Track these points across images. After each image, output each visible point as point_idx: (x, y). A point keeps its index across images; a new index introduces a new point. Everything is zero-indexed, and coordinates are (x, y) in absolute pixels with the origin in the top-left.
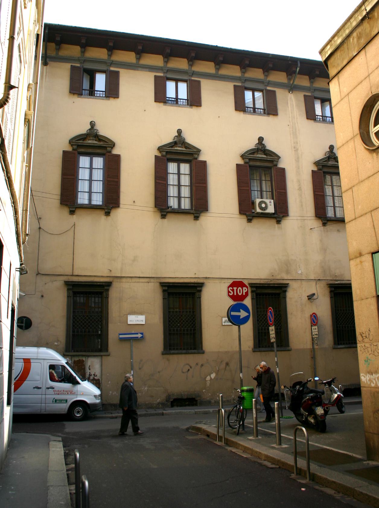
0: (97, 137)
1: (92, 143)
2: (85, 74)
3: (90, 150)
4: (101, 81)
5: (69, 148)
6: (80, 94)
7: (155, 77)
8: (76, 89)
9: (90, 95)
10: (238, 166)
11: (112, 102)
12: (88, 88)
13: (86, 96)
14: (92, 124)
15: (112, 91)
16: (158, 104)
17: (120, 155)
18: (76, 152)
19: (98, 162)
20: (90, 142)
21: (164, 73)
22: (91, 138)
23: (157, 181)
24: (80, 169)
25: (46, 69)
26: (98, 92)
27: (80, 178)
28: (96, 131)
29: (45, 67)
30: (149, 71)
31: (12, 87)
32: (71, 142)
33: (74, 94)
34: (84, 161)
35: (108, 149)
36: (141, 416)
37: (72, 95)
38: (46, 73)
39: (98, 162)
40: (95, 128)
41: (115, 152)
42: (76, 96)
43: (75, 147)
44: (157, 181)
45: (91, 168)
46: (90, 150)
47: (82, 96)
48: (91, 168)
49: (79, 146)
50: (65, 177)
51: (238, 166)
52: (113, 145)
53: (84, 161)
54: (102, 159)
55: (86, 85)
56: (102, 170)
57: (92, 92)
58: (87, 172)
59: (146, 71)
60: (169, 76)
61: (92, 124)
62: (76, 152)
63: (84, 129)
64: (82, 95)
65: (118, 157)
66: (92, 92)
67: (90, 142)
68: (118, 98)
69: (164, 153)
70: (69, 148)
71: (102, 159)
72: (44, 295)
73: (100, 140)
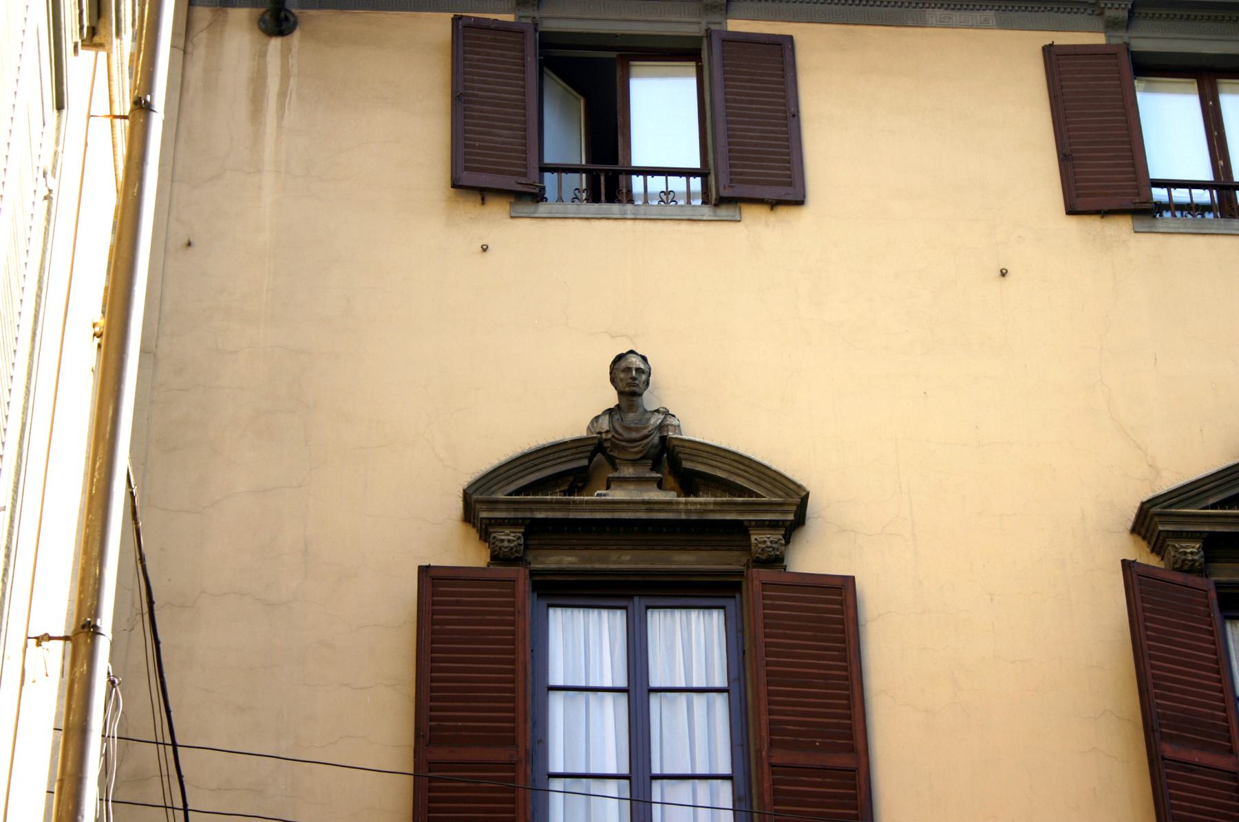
0: (672, 458)
1: (637, 512)
2: (555, 89)
3: (623, 560)
4: (664, 116)
5: (461, 551)
6: (527, 196)
7: (1050, 52)
8: (490, 171)
9: (594, 198)
10: (431, 579)
11: (757, 231)
12: (578, 156)
13: (572, 208)
14: (629, 376)
15: (754, 164)
16: (1093, 224)
17: (851, 580)
18: (520, 575)
19: (690, 644)
20: (617, 494)
21: (1111, 26)
22: (628, 471)
23: (1168, 750)
24: (557, 703)
25: (285, 54)
26: (657, 184)
27: (557, 766)
28: (656, 420)
29: (275, 43)
30: (1003, 25)
31: (45, 198)
32: (480, 504)
33: (484, 193)
34: (581, 643)
35: (756, 537)
36: (262, 55)
37: (470, 208)
38: (285, 76)
39: (690, 644)
40: (650, 400)
41: (812, 557)
42: (498, 210)
43: (509, 537)
44: (1168, 750)
45: (638, 691)
46: (623, 560)
47: (543, 208)
48: (638, 691)
49: (541, 532)
50: (441, 754)
51: (431, 579)
52: (791, 509)
53: (581, 643)
54: (716, 619)
55: (563, 140)
56: (720, 702)
57: (607, 176)
58: (610, 717)
59: (984, 25)
60: (1151, 39)
61: (629, 376)
62: (520, 575)
63: (571, 406)
64: (538, 196)
65: (840, 591)
66: (607, 176)
67: (617, 494)
68: (799, 202)
69: (1192, 548)
70: (461, 551)
71: (716, 619)
72: (487, 254)
73: (690, 483)
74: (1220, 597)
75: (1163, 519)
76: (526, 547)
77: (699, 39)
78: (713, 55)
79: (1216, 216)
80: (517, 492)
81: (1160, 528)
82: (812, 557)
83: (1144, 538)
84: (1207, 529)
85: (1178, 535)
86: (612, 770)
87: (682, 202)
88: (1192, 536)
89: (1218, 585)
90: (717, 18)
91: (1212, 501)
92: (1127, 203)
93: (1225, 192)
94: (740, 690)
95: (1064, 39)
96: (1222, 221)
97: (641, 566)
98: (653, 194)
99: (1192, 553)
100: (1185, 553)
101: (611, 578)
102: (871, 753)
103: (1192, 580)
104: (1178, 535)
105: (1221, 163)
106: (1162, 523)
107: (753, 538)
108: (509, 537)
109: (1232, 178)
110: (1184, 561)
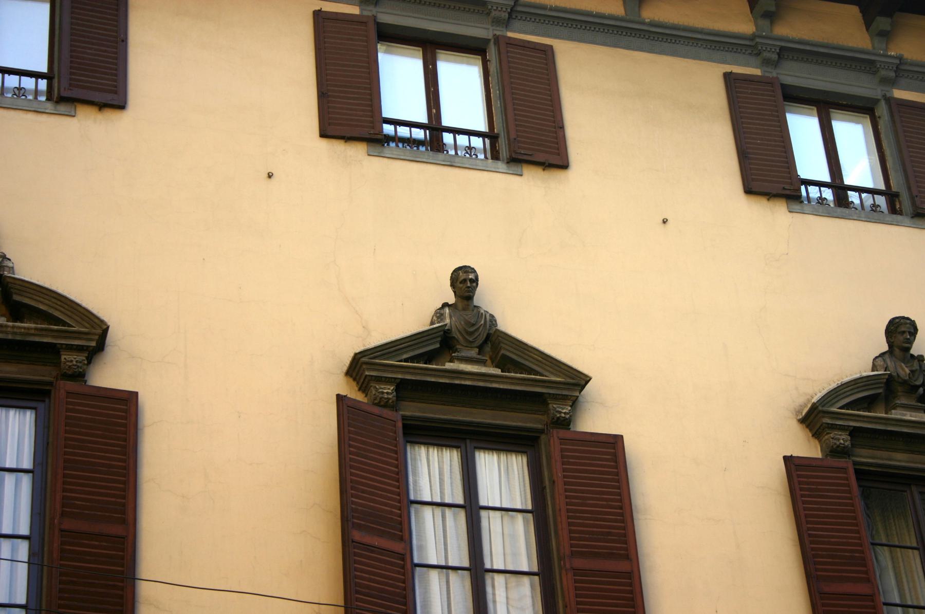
75: (368, 367)
77: (487, 41)
81: (367, 373)
84: (400, 376)
85: (379, 380)
88: (388, 381)
91: (405, 356)
103: (387, 413)
104: (379, 380)
106: (369, 369)
110: (558, 418)
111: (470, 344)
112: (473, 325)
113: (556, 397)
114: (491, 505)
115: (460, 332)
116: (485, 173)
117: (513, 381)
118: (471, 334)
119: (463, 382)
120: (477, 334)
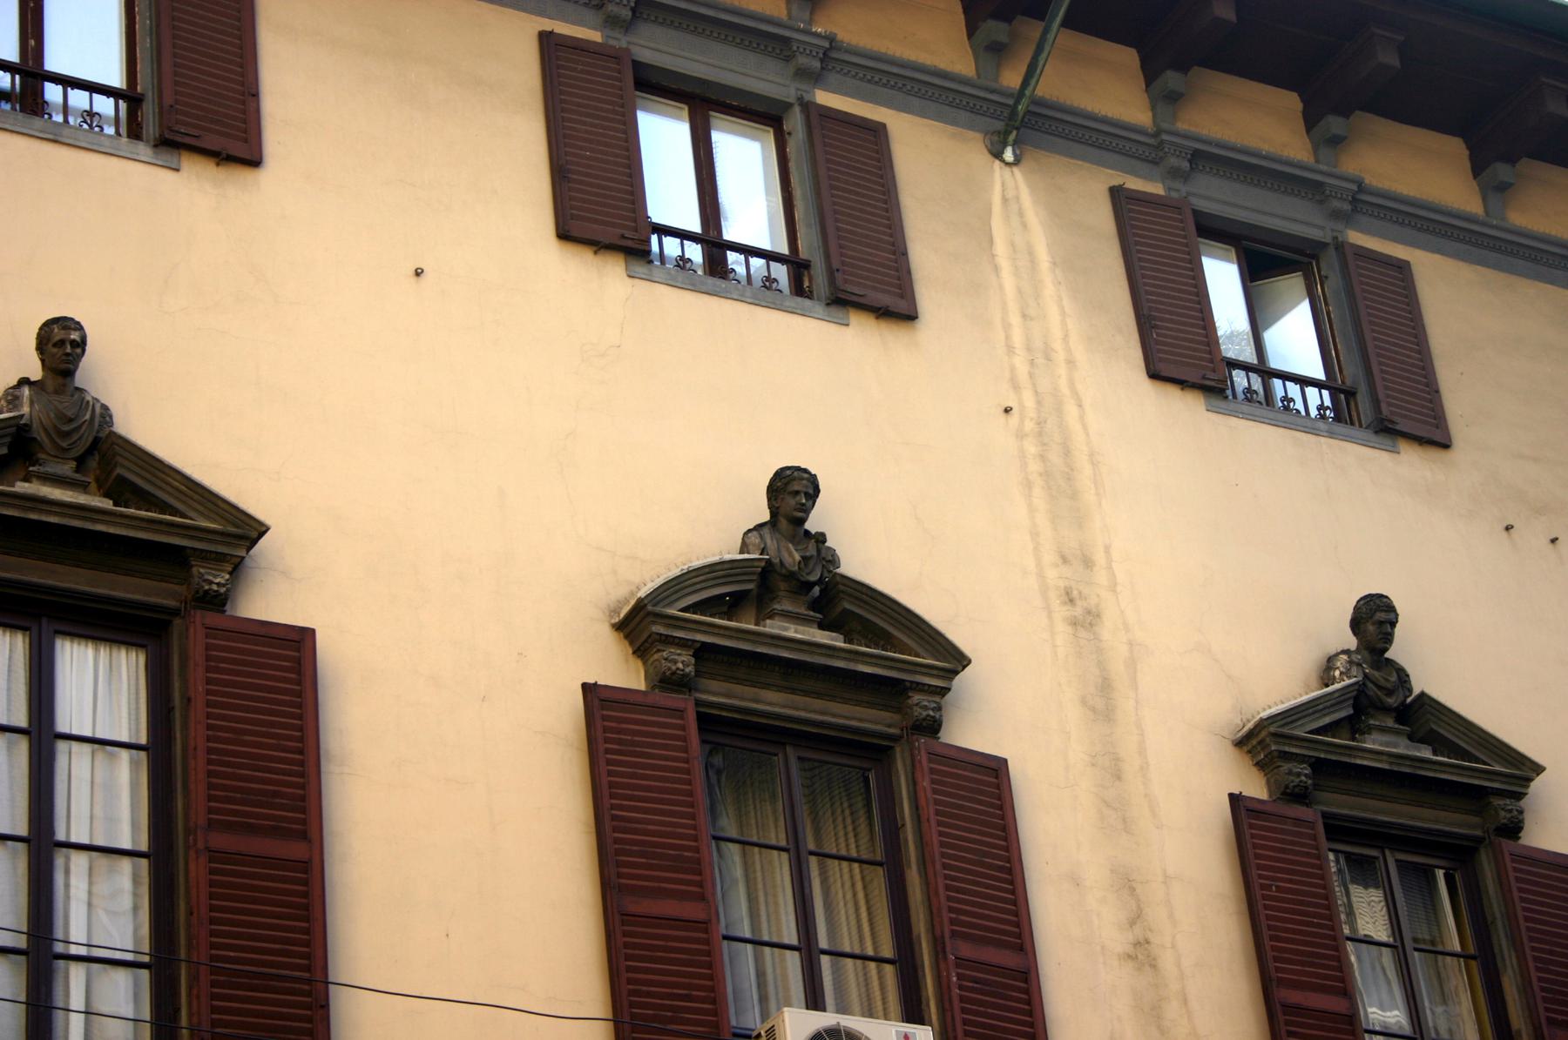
0: (1423, 717)
7: (545, 38)
15: (850, 264)
21: (612, 22)
35: (199, 570)
61: (61, 344)
68: (253, 161)
70: (621, 671)
73: (121, 491)
74: (701, 718)
76: (698, 673)
78: (1329, 265)
79: (14, 109)
80: (1317, 731)
82: (268, 600)
83: (626, 637)
85: (668, 641)
86: (126, 844)
87: (59, 118)
88: (1301, 759)
89: (1325, 815)
90: (1339, 226)
92: (611, 235)
93: (715, 250)
94: (161, 751)
95: (1135, 184)
96: (20, 116)
97: (153, 600)
98: (76, 110)
99: (218, 584)
100: (211, 583)
101: (832, 733)
102: (1259, 986)
104: (668, 641)
105: (32, 42)
107: (195, 570)
108: (683, 661)
109: (42, 64)
110: (206, 592)
111: (61, 454)
112: (71, 420)
113: (205, 556)
114: (75, 732)
115: (45, 430)
116: (114, 160)
117: (134, 521)
118: (67, 434)
119: (44, 518)
120: (75, 437)
